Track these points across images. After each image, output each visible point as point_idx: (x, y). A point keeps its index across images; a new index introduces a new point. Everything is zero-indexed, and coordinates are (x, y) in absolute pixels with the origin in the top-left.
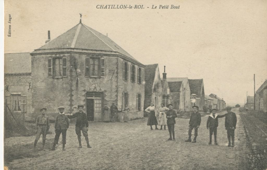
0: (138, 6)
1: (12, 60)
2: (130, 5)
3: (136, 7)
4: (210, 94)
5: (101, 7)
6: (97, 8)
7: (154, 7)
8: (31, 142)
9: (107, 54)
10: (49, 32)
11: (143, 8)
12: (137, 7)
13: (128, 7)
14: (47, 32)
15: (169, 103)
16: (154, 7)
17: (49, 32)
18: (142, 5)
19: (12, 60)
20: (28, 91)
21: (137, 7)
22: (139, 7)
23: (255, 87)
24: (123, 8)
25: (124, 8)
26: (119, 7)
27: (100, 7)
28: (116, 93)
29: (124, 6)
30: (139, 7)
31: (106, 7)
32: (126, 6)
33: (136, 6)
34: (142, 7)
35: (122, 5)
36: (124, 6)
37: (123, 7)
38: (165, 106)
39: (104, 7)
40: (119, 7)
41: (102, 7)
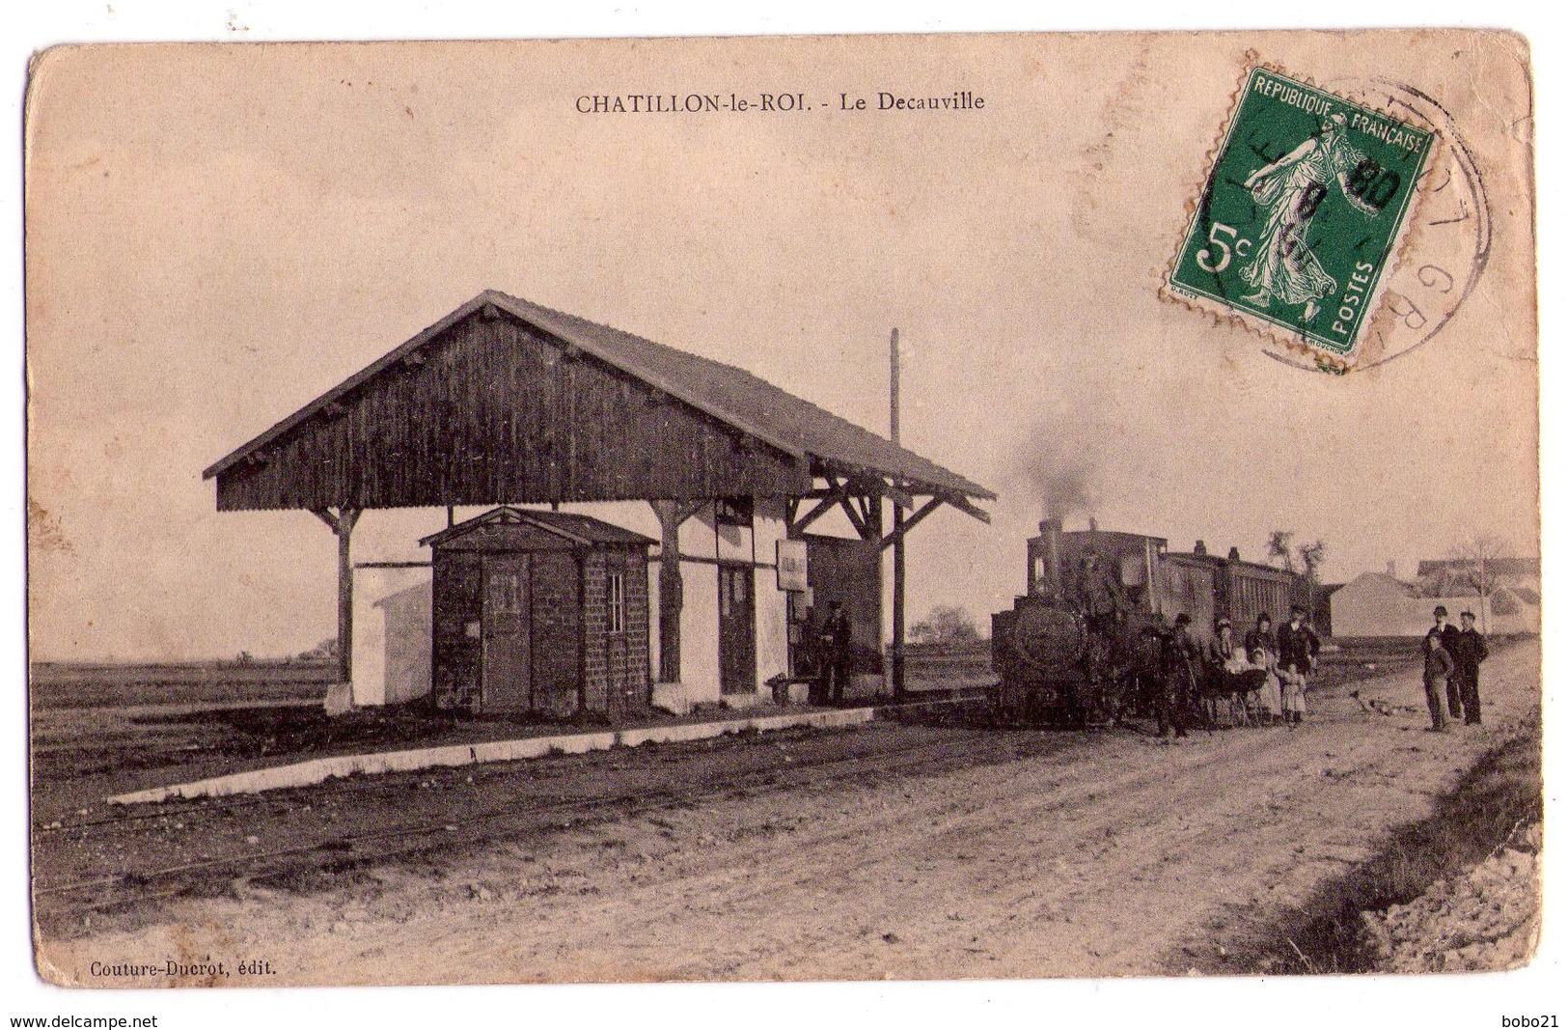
0: (895, 105)
1: (791, 505)
3: (767, 103)
7: (850, 102)
8: (1416, 633)
10: (895, 332)
12: (774, 103)
14: (889, 333)
16: (850, 102)
17: (895, 332)
19: (791, 505)
21: (774, 103)
23: (384, 565)
25: (708, 110)
27: (591, 103)
31: (621, 105)
32: (714, 100)
35: (787, 91)
36: (704, 100)
38: (321, 705)
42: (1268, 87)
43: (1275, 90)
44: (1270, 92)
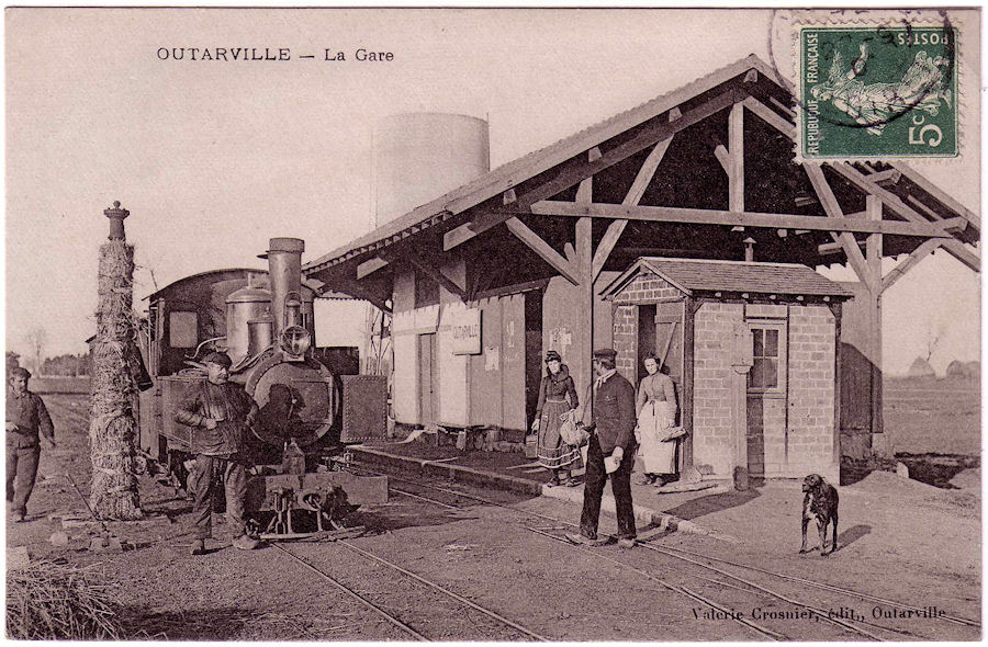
10: (390, 56)
43: (813, 139)
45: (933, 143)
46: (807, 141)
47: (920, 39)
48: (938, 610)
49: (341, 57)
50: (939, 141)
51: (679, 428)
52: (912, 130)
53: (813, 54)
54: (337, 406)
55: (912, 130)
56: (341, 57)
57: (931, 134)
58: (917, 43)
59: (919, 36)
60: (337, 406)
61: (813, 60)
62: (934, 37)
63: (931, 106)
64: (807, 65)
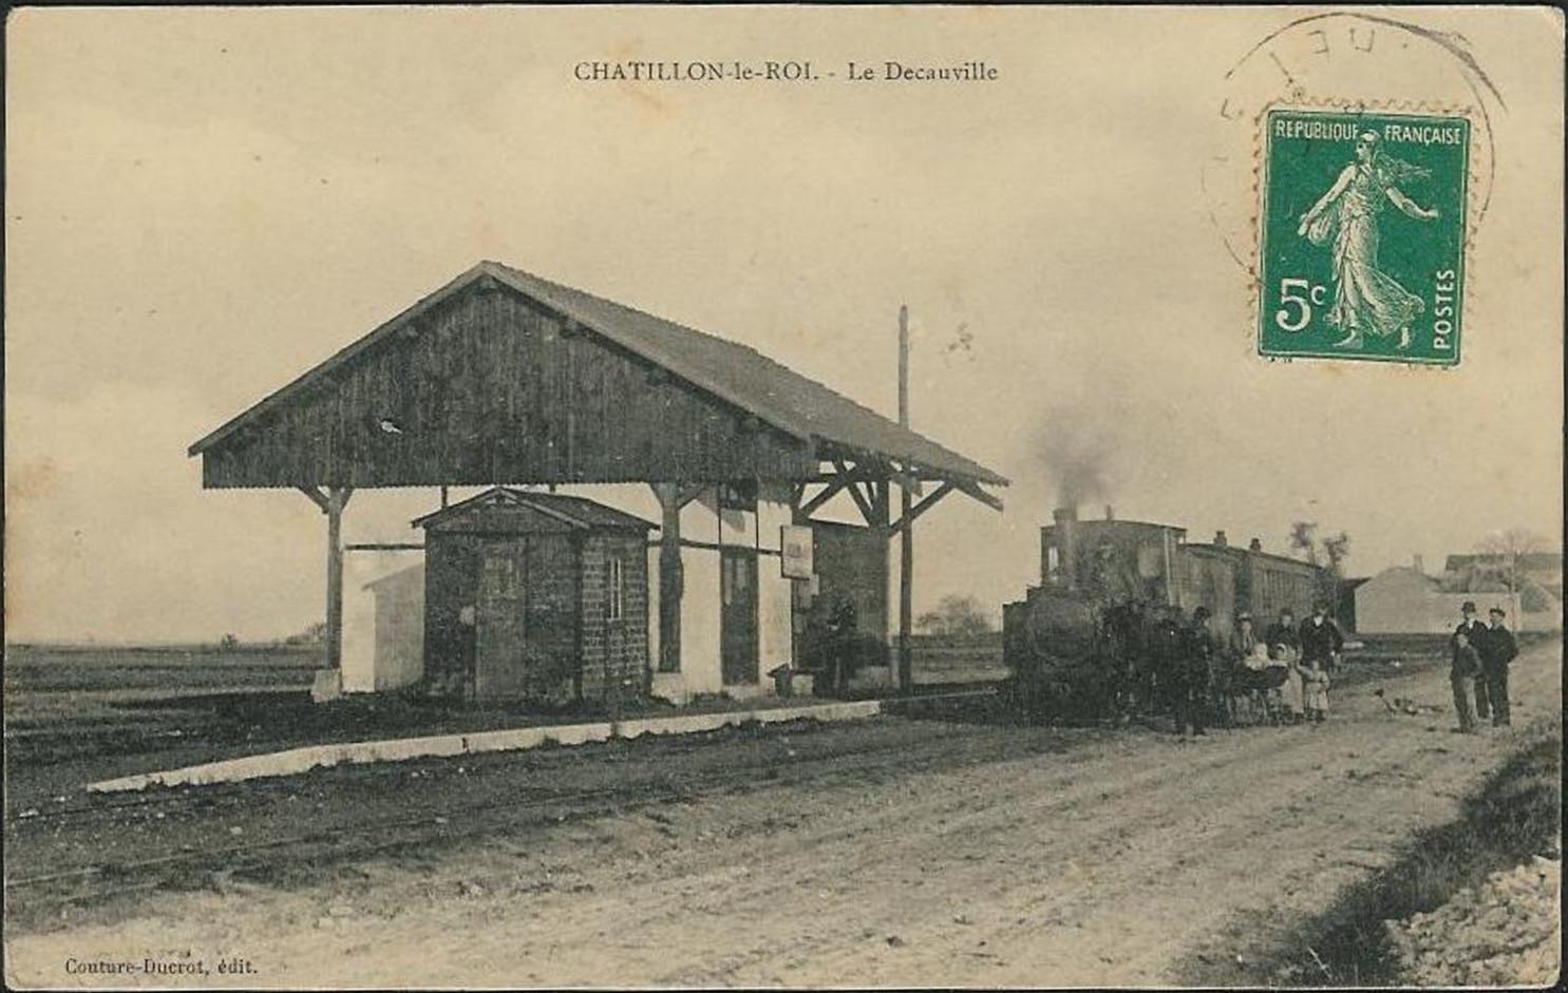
2: (737, 64)
4: (1444, 563)
5: (596, 71)
6: (577, 75)
7: (858, 72)
9: (240, 417)
10: (904, 308)
11: (812, 76)
12: (780, 72)
13: (730, 74)
15: (621, 637)
16: (858, 72)
18: (807, 65)
20: (1178, 822)
21: (780, 72)
22: (792, 71)
24: (707, 76)
26: (683, 72)
28: (126, 654)
29: (707, 67)
30: (792, 71)
32: (717, 68)
33: (773, 67)
34: (804, 71)
37: (785, 71)
39: (610, 75)
40: (683, 72)
41: (601, 75)
42: (1290, 129)
43: (1298, 129)
44: (1293, 132)
45: (1282, 315)
46: (1295, 120)
47: (1442, 305)
48: (987, 68)
49: (868, 75)
50: (1286, 327)
51: (612, 808)
52: (1304, 283)
53: (1430, 135)
54: (146, 713)
55: (1304, 283)
56: (868, 75)
57: (1295, 314)
58: (1439, 299)
59: (1448, 304)
60: (146, 713)
61: (1419, 136)
62: (1440, 327)
63: (1339, 314)
64: (1412, 125)
